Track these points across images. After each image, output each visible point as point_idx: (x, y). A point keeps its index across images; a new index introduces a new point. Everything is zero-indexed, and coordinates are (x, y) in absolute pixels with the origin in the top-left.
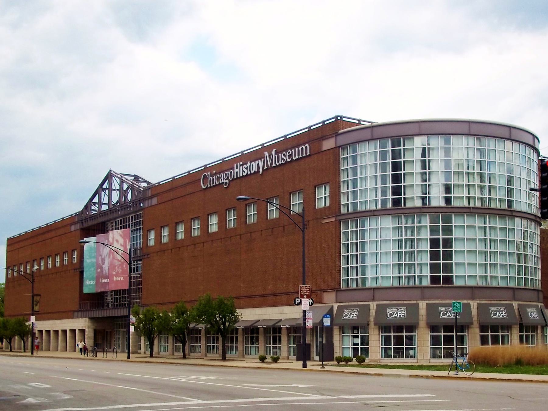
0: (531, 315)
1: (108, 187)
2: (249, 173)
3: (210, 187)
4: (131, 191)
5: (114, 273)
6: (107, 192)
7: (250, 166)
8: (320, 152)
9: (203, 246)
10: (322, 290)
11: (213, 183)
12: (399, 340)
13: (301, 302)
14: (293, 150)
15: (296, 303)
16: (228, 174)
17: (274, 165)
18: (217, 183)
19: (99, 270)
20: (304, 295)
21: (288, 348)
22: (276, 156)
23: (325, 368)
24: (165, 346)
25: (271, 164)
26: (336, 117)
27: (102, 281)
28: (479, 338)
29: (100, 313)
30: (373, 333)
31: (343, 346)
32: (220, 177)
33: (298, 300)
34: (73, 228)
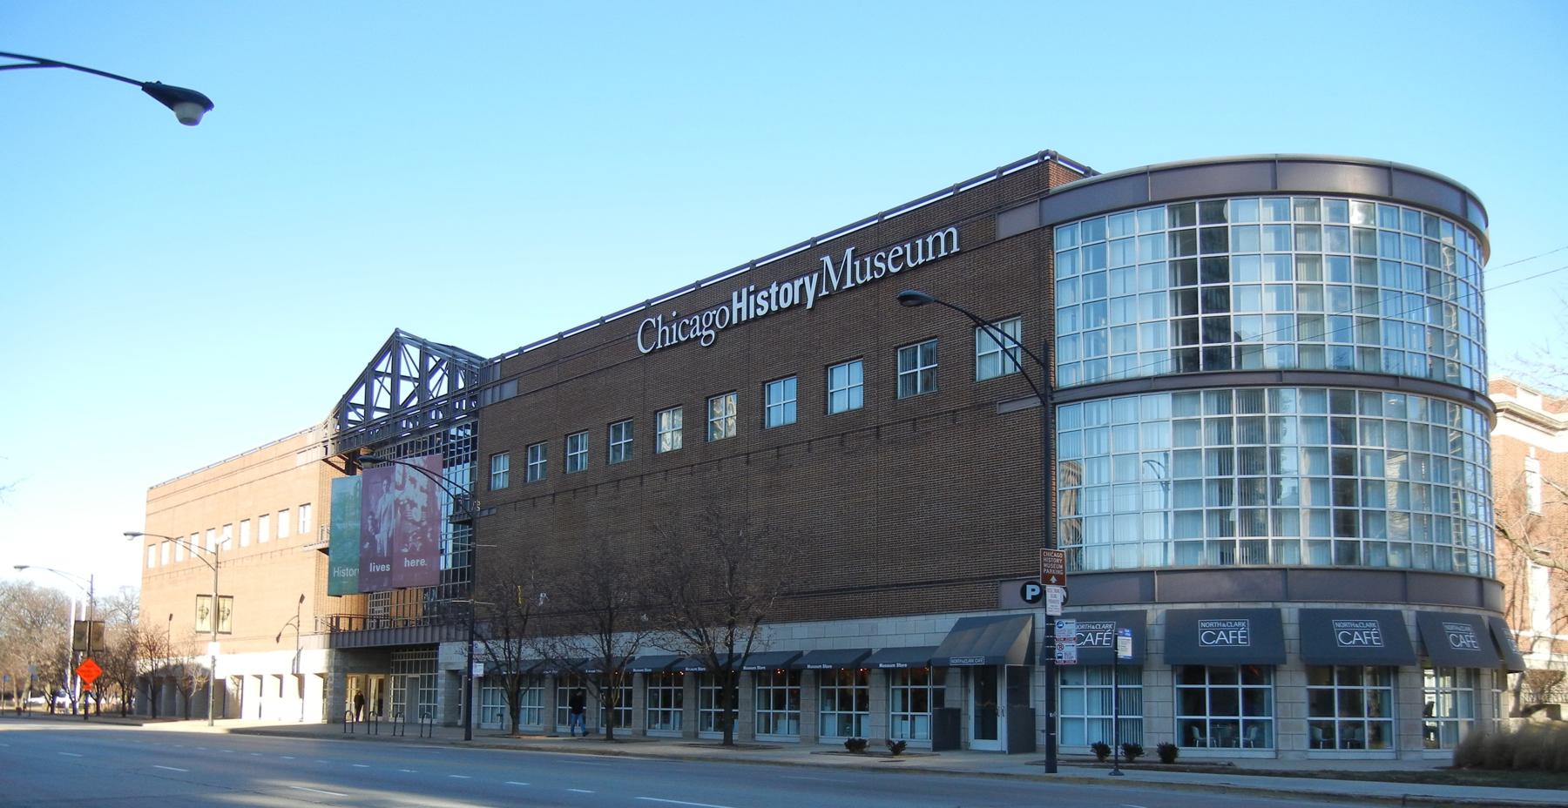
0: (1457, 641)
1: (389, 371)
2: (774, 308)
3: (663, 349)
4: (446, 378)
5: (405, 550)
6: (387, 382)
7: (778, 293)
8: (993, 243)
9: (641, 483)
10: (998, 577)
11: (671, 340)
12: (1224, 702)
13: (1043, 593)
14: (908, 246)
15: (1029, 598)
16: (714, 316)
17: (849, 284)
18: (682, 339)
19: (367, 546)
20: (1051, 575)
21: (887, 717)
22: (857, 263)
23: (1123, 775)
24: (532, 713)
25: (842, 281)
26: (1043, 154)
27: (373, 568)
28: (1304, 697)
29: (429, 633)
30: (1154, 683)
31: (1063, 716)
32: (691, 324)
33: (1033, 590)
34: (302, 459)
